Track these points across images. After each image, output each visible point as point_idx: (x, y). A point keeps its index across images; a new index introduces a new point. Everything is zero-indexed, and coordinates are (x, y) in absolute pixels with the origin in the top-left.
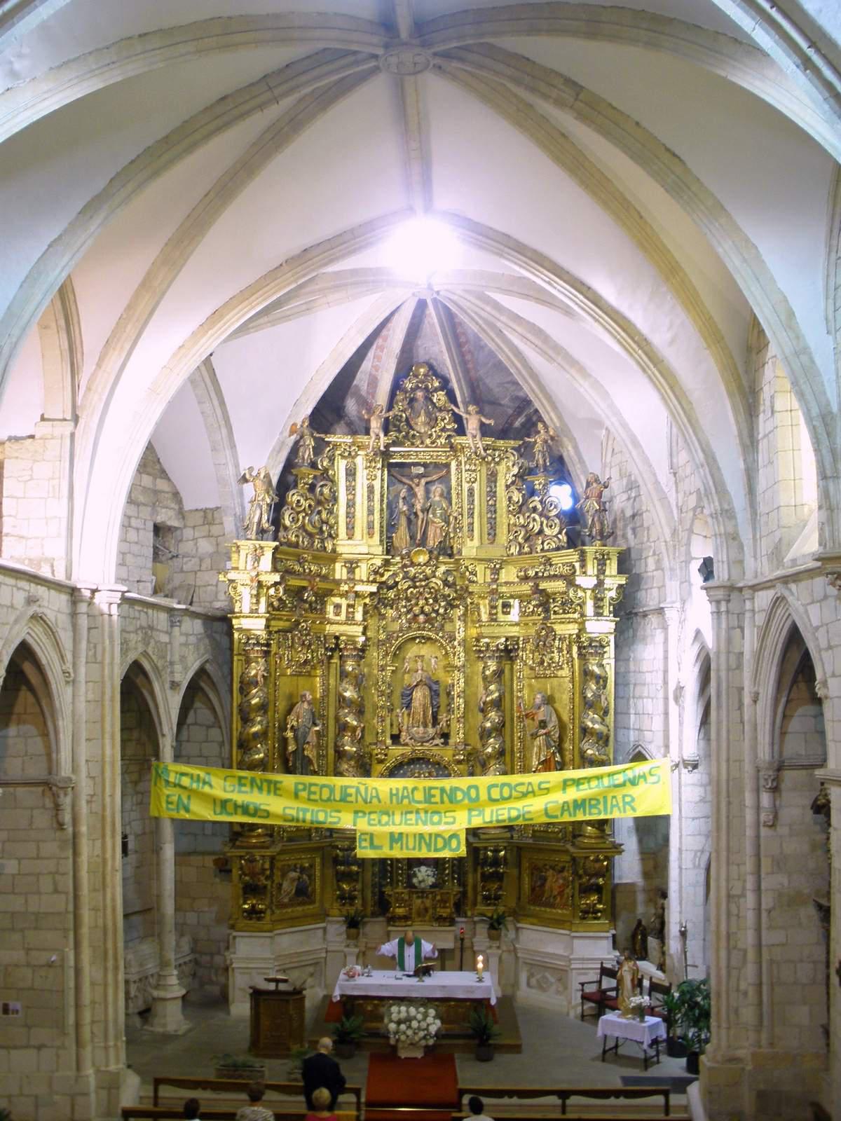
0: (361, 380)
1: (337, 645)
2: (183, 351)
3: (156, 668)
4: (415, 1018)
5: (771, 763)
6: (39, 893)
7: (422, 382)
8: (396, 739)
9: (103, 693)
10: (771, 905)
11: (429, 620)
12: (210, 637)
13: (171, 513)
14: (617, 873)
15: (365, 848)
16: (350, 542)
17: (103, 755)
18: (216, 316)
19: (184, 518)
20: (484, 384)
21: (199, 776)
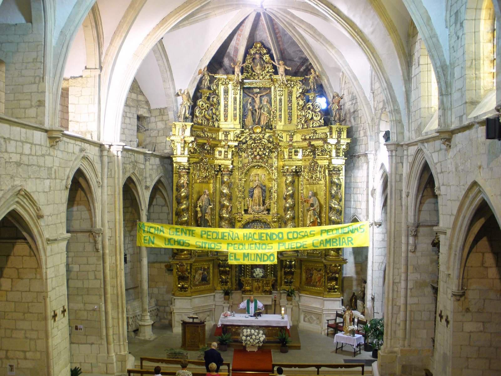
0: (231, 50)
1: (220, 169)
2: (149, 37)
3: (138, 180)
4: (254, 334)
5: (414, 224)
6: (88, 279)
7: (258, 50)
8: (246, 211)
9: (115, 191)
10: (412, 287)
11: (261, 158)
12: (162, 166)
13: (145, 110)
14: (344, 272)
15: (233, 260)
16: (226, 123)
17: (115, 219)
18: (164, 21)
19: (151, 113)
20: (287, 51)
21: (158, 228)
